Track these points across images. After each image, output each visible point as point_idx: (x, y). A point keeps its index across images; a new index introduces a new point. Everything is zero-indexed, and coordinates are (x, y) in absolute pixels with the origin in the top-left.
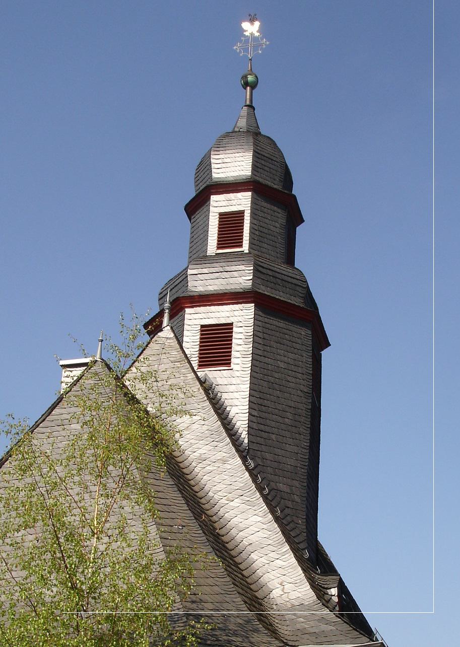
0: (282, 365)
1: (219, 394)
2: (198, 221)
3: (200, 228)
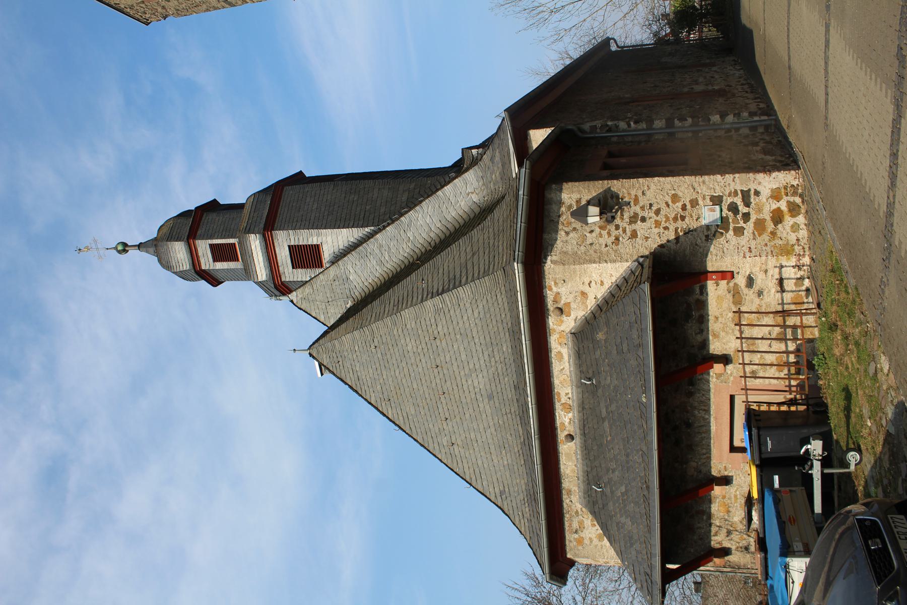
0: (315, 206)
1: (341, 251)
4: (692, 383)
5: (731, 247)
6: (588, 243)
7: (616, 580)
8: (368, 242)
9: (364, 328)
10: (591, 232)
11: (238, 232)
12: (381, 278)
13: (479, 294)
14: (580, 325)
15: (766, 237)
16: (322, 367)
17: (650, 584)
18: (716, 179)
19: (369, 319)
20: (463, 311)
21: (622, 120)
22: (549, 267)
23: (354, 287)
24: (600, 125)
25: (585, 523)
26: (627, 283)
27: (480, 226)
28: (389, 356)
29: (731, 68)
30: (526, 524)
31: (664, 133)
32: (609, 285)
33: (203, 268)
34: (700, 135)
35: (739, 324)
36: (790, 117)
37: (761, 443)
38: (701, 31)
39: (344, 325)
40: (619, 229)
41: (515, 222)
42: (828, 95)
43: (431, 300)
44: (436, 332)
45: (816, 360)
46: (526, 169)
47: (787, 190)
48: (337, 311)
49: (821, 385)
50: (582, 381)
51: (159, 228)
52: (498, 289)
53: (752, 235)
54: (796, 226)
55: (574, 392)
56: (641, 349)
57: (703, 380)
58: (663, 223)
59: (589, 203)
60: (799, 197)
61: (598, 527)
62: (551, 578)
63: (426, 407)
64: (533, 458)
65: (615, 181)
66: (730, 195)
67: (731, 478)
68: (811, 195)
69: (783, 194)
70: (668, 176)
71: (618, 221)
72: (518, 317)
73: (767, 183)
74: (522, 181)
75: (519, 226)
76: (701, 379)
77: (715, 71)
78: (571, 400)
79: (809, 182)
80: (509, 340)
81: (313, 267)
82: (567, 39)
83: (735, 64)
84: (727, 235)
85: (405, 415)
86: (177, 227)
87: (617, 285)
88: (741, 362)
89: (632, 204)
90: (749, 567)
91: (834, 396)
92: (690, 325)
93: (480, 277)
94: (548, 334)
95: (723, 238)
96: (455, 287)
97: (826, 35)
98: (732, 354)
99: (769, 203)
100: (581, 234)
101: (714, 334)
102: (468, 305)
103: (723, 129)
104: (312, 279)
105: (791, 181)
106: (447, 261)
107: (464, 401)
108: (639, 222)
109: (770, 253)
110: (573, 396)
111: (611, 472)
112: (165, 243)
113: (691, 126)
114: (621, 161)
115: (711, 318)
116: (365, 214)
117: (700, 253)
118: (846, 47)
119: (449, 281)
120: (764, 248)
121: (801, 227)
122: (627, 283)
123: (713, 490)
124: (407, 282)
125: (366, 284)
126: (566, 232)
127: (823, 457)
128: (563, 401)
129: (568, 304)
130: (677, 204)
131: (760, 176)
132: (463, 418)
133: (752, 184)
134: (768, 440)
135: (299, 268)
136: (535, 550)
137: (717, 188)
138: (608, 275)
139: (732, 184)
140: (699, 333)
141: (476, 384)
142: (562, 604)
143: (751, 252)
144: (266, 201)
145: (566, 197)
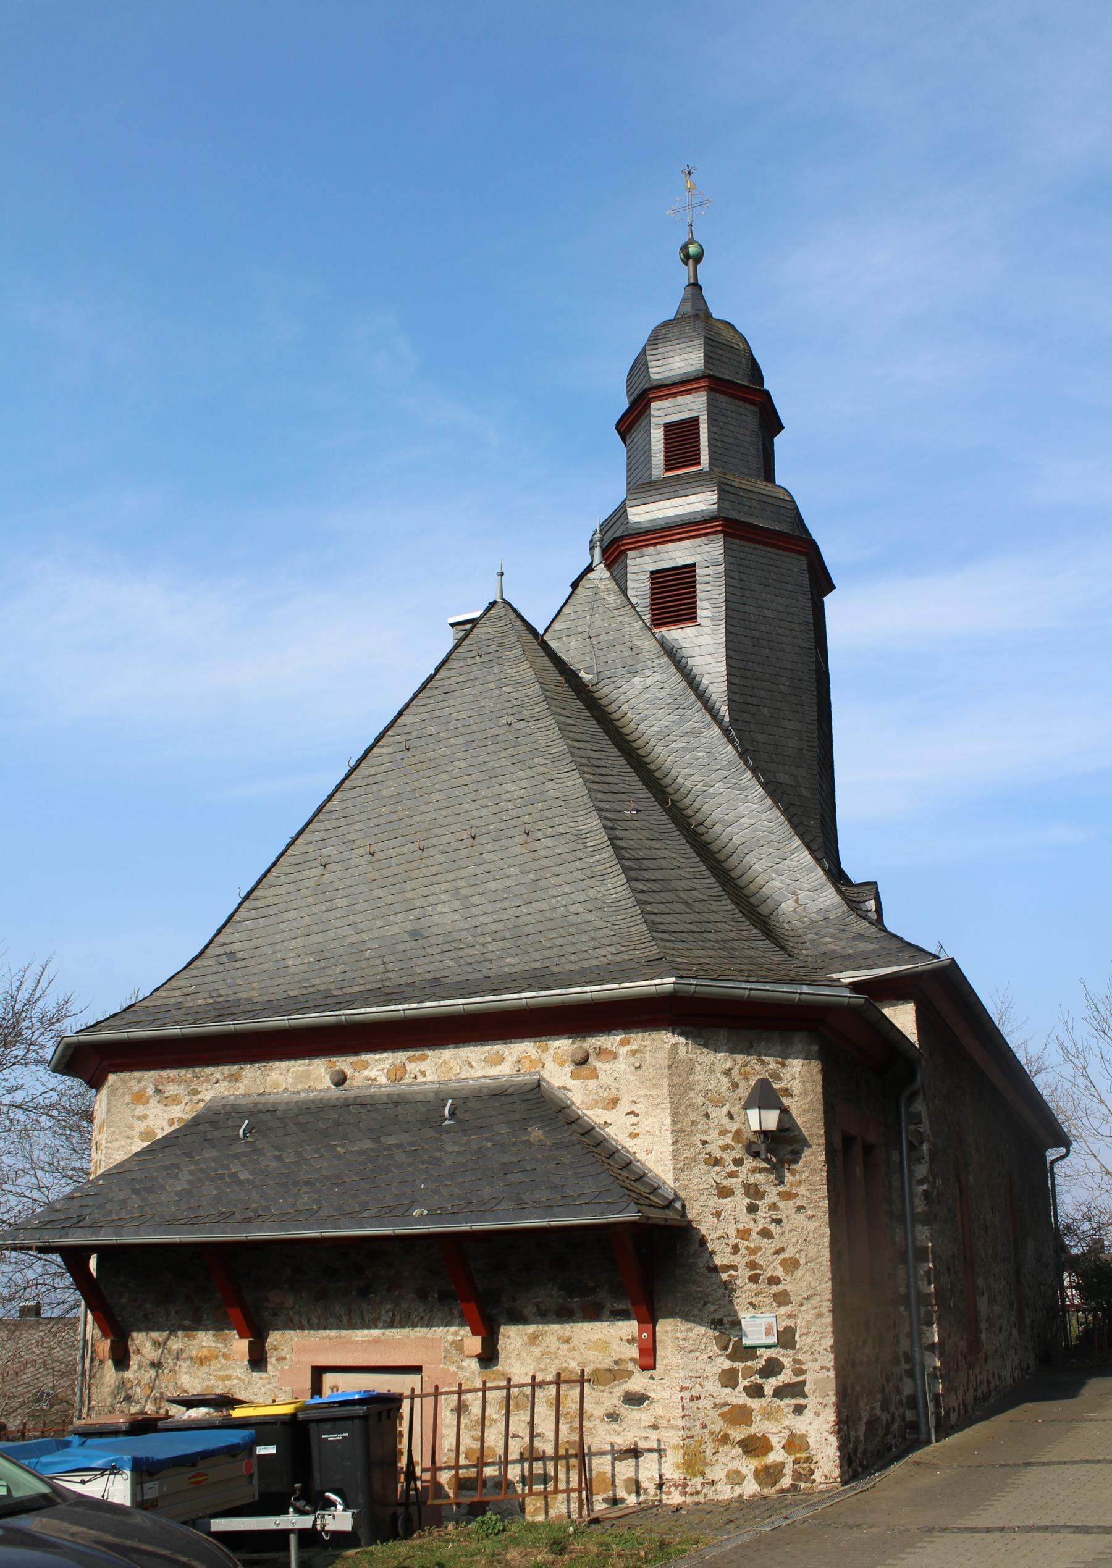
0: (769, 614)
1: (684, 660)
2: (636, 440)
3: (640, 449)
4: (445, 1297)
5: (700, 1365)
6: (710, 1110)
7: (53, 1164)
8: (704, 711)
9: (545, 702)
10: (730, 1116)
11: (720, 470)
12: (636, 735)
13: (614, 914)
14: (555, 1095)
15: (719, 1426)
16: (469, 626)
17: (63, 1225)
18: (826, 1337)
19: (562, 712)
20: (581, 885)
21: (931, 1171)
22: (666, 1040)
23: (618, 684)
24: (921, 1130)
25: (175, 1107)
26: (635, 1181)
27: (741, 915)
28: (492, 748)
29: (1016, 1363)
30: (172, 1000)
31: (906, 1245)
32: (630, 1149)
33: (654, 405)
34: (902, 1308)
35: (558, 1381)
36: (936, 1466)
37: (337, 1423)
38: (1078, 1308)
39: (550, 665)
40: (735, 1165)
41: (751, 979)
42: (988, 1532)
43: (601, 825)
44: (540, 835)
45: (494, 1518)
46: (850, 997)
47: (805, 1462)
48: (572, 653)
49: (446, 1527)
50: (450, 1101)
51: (729, 324)
52: (623, 949)
53: (723, 1401)
54: (738, 1479)
55: (427, 1086)
56: (513, 1205)
57: (449, 1318)
58: (746, 1243)
59: (784, 1111)
60: (791, 1485)
61: (169, 1130)
62: (68, 1046)
63: (394, 817)
64: (300, 1012)
65: (823, 1158)
66: (796, 1361)
67: (263, 1368)
68: (797, 1505)
69: (798, 1455)
70: (831, 1252)
71: (750, 1163)
72: (571, 985)
73: (817, 1427)
74: (827, 991)
75: (744, 985)
76: (451, 1314)
77: (1011, 1334)
78: (411, 1080)
79: (821, 1502)
80: (528, 968)
81: (653, 610)
82: (1068, 1070)
83: (1022, 1370)
84: (723, 1358)
85: (379, 778)
86: (733, 356)
87: (631, 1162)
88: (488, 1385)
89: (781, 1188)
90: (93, 1403)
91: (427, 1550)
92: (554, 1292)
93: (647, 916)
94: (537, 1039)
95: (718, 1351)
96: (625, 870)
97: (1098, 1527)
98: (499, 1368)
99: (781, 1432)
100: (727, 1098)
101: (536, 1337)
102: (592, 893)
103: (912, 1347)
104: (633, 607)
105: (820, 1470)
106: (674, 855)
107: (408, 886)
108: (748, 1201)
109: (689, 1434)
110: (419, 1084)
111: (277, 1153)
112: (702, 333)
113: (919, 1293)
114: (858, 1169)
115: (567, 1329)
116: (753, 705)
117: (689, 1311)
118: (1081, 1562)
119: (638, 859)
120: (698, 1423)
121: (736, 1487)
122: (635, 1181)
123: (242, 1336)
124: (634, 783)
125: (625, 707)
126: (730, 1070)
127: (320, 1532)
128: (410, 1067)
129: (594, 1074)
130: (781, 1269)
131: (830, 1415)
132: (375, 885)
133: (815, 1401)
134: (344, 1435)
135: (652, 584)
136: (123, 1015)
137: (810, 1339)
138: (650, 1147)
139: (817, 1366)
140: (539, 1310)
141: (440, 908)
142: (1, 1071)
143: (692, 1400)
144: (780, 522)
145: (794, 1070)
